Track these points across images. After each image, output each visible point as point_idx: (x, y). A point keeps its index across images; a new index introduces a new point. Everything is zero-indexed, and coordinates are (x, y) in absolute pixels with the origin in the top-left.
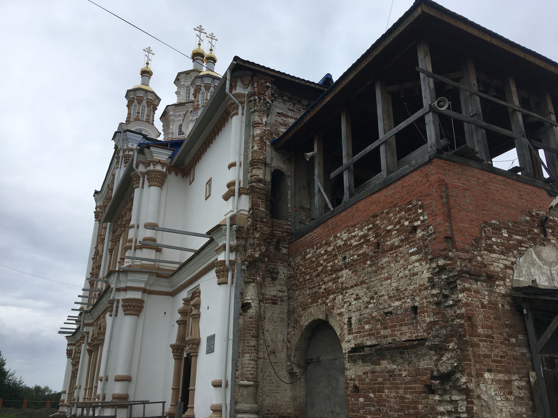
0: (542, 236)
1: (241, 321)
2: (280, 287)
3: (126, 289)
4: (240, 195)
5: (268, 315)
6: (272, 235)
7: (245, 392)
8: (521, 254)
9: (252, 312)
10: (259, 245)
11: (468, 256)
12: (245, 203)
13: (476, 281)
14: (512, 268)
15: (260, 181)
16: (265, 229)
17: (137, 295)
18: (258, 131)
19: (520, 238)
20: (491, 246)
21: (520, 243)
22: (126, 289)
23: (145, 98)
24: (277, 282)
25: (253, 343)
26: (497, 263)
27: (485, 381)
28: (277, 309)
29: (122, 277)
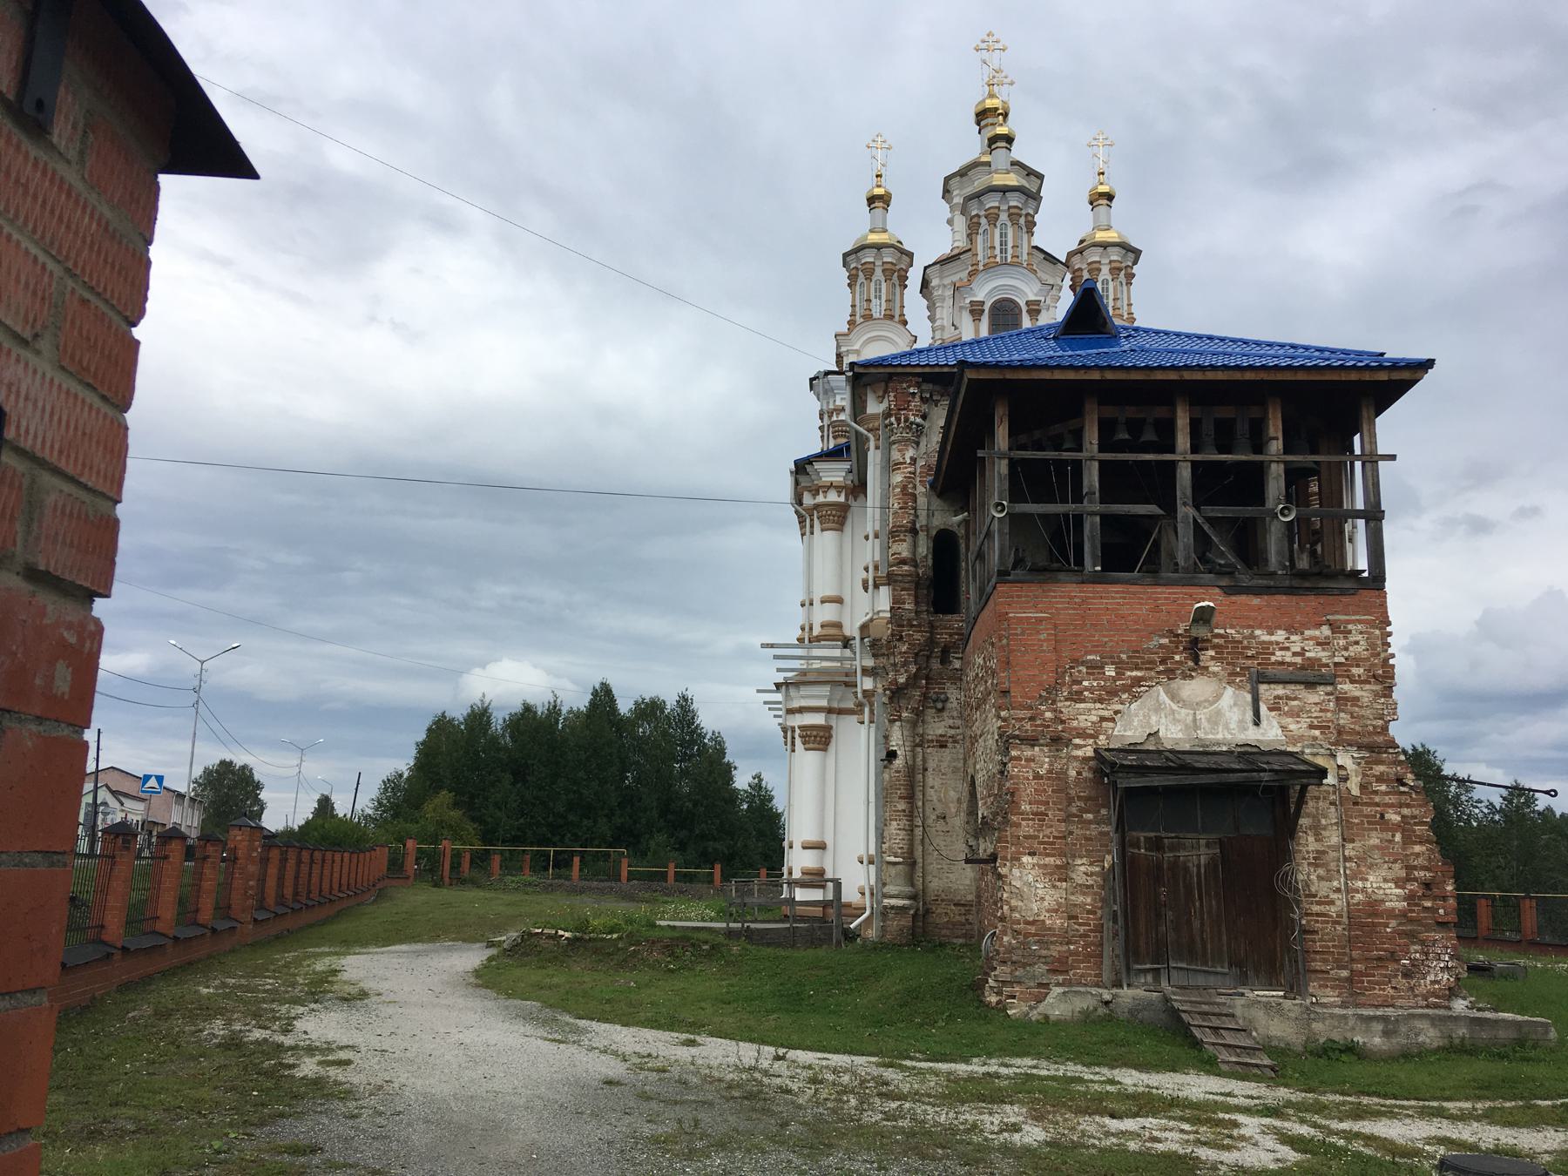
0: (1191, 663)
1: (886, 776)
2: (951, 722)
3: (801, 710)
4: (876, 586)
5: (931, 765)
6: (931, 642)
7: (893, 871)
8: (1136, 697)
9: (898, 763)
10: (905, 664)
11: (1028, 714)
12: (884, 599)
13: (1033, 746)
14: (1113, 720)
15: (903, 562)
16: (917, 636)
17: (819, 719)
18: (898, 478)
19: (1139, 674)
20: (1080, 693)
21: (1137, 682)
22: (801, 710)
23: (879, 263)
24: (945, 714)
25: (902, 806)
26: (1085, 715)
27: (1022, 866)
28: (946, 754)
29: (793, 692)
